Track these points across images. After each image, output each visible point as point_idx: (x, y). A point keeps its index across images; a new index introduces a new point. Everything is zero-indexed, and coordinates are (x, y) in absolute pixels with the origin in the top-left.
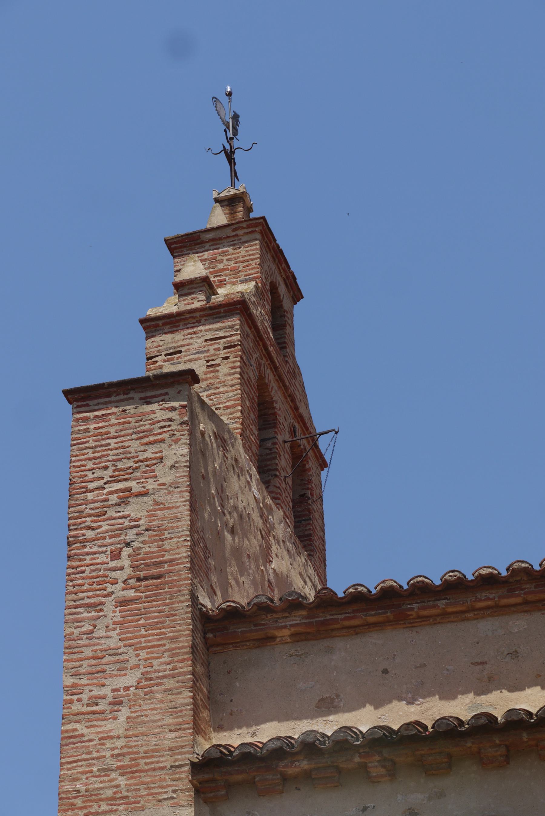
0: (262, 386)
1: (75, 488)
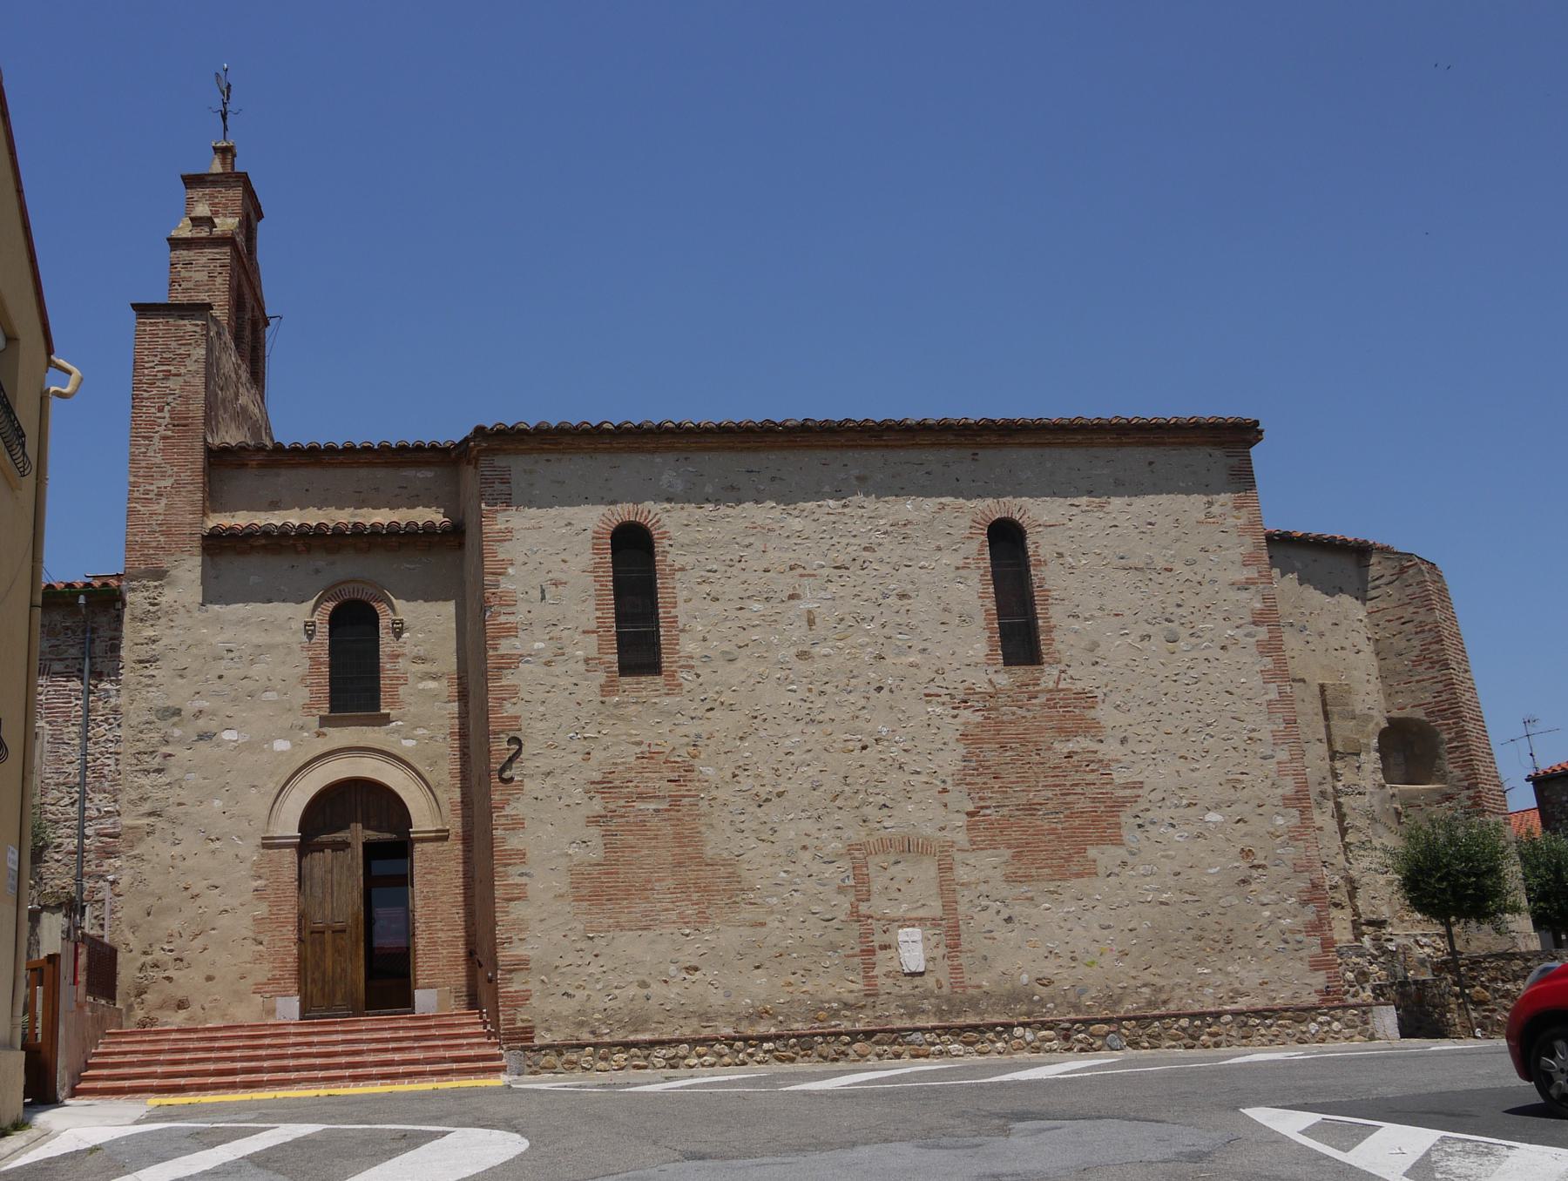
0: (239, 286)
1: (137, 365)
